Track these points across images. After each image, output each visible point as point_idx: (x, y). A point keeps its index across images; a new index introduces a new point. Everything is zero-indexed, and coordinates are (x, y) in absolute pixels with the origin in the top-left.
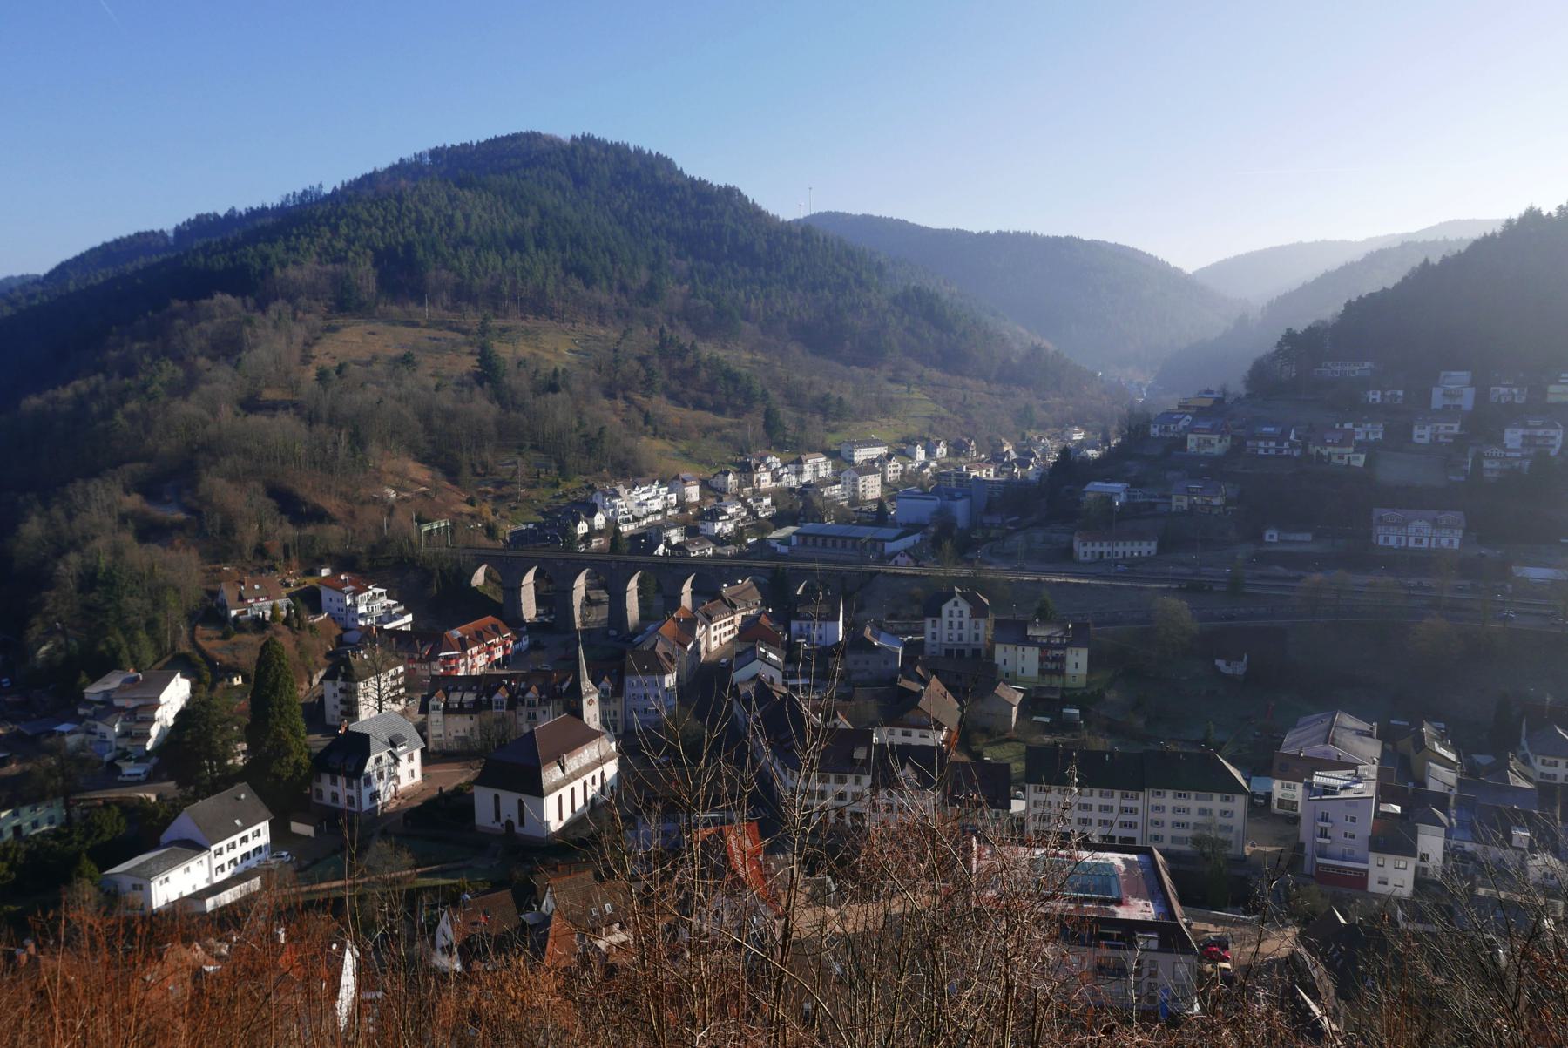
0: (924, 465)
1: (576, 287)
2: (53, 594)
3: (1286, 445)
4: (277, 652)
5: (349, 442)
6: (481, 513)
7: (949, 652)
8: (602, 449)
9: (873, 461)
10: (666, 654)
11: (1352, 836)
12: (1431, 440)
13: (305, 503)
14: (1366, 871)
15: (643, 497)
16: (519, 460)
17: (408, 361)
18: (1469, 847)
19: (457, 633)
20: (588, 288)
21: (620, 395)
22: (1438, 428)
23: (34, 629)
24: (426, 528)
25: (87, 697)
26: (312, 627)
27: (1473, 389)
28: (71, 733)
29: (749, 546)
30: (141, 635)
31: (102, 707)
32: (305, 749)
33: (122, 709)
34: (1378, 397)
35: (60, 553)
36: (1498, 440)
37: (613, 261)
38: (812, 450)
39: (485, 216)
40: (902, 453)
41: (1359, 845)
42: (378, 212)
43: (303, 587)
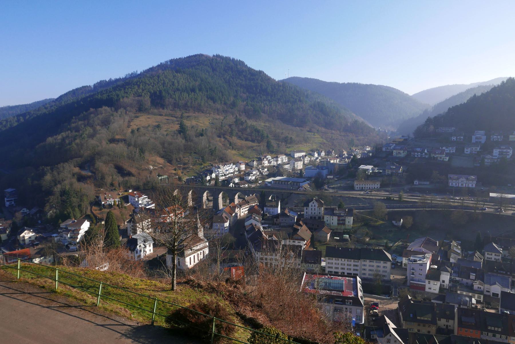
0: (317, 158)
1: (210, 103)
2: (52, 197)
3: (424, 154)
4: (112, 215)
5: (139, 152)
6: (178, 173)
7: (311, 217)
8: (216, 153)
9: (300, 157)
10: (226, 217)
11: (421, 275)
12: (470, 153)
13: (126, 170)
14: (425, 285)
15: (227, 168)
16: (190, 157)
17: (159, 127)
18: (457, 279)
19: (167, 209)
20: (214, 103)
21: (222, 136)
22: (472, 149)
23: (47, 207)
24: (160, 178)
25: (61, 226)
26: (125, 207)
27: (486, 136)
28: (56, 237)
29: (259, 184)
30: (77, 209)
31: (65, 229)
32: (120, 243)
33: (70, 230)
34: (455, 139)
35: (56, 185)
36: (491, 153)
37: (222, 95)
38: (282, 153)
39: (184, 81)
40: (310, 154)
41: (423, 278)
42: (151, 81)
43: (124, 195)
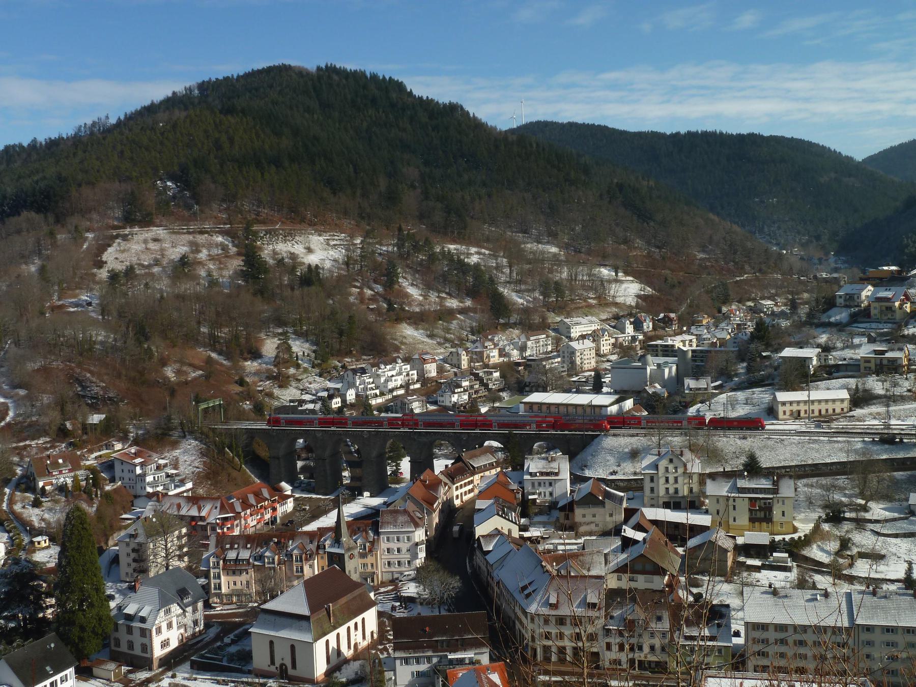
37: (355, 172)
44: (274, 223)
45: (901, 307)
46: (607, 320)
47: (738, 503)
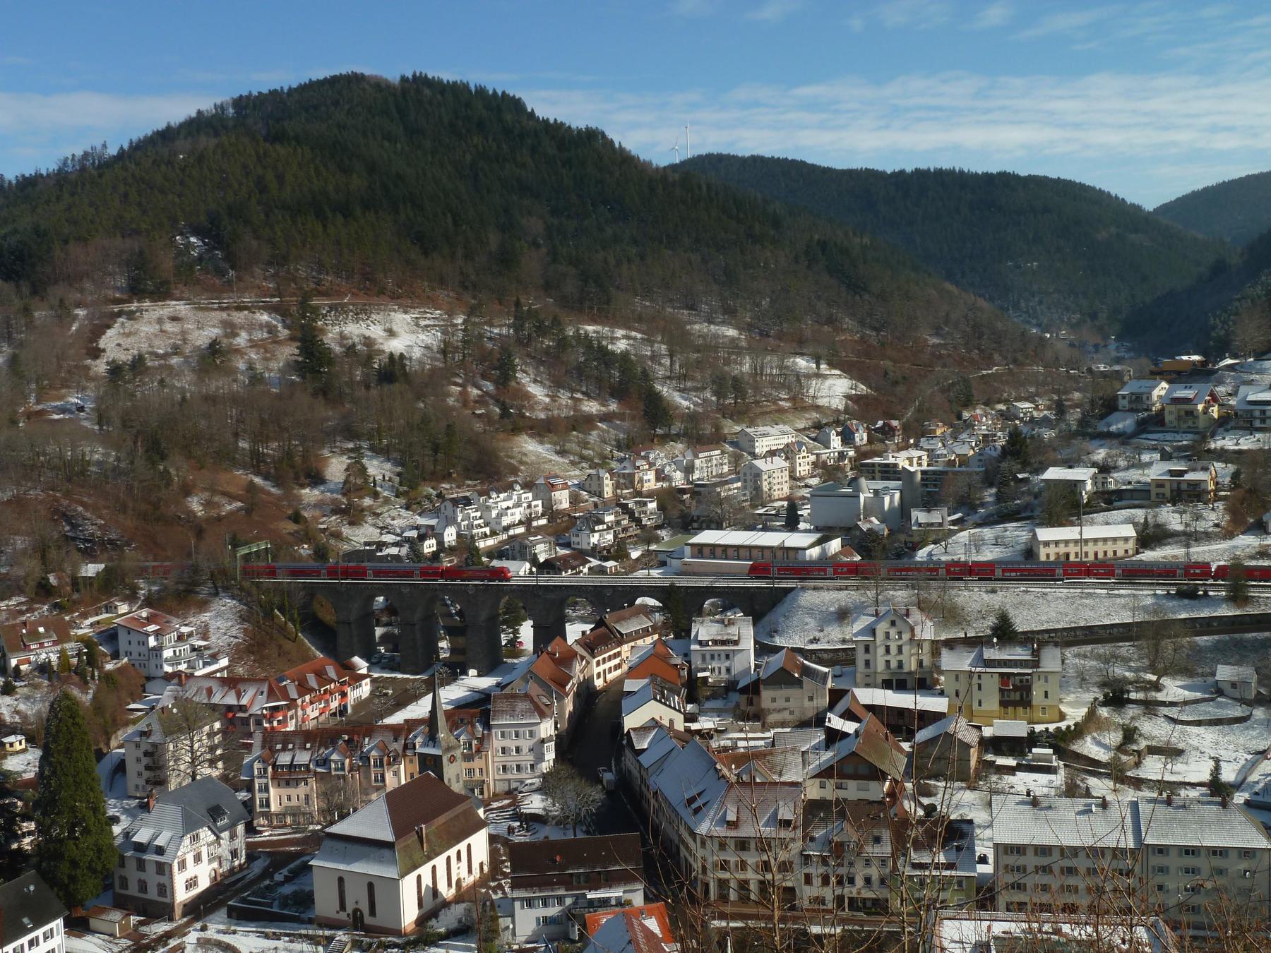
37: (455, 223)
44: (341, 294)
45: (1205, 411)
46: (805, 429)
47: (985, 681)
